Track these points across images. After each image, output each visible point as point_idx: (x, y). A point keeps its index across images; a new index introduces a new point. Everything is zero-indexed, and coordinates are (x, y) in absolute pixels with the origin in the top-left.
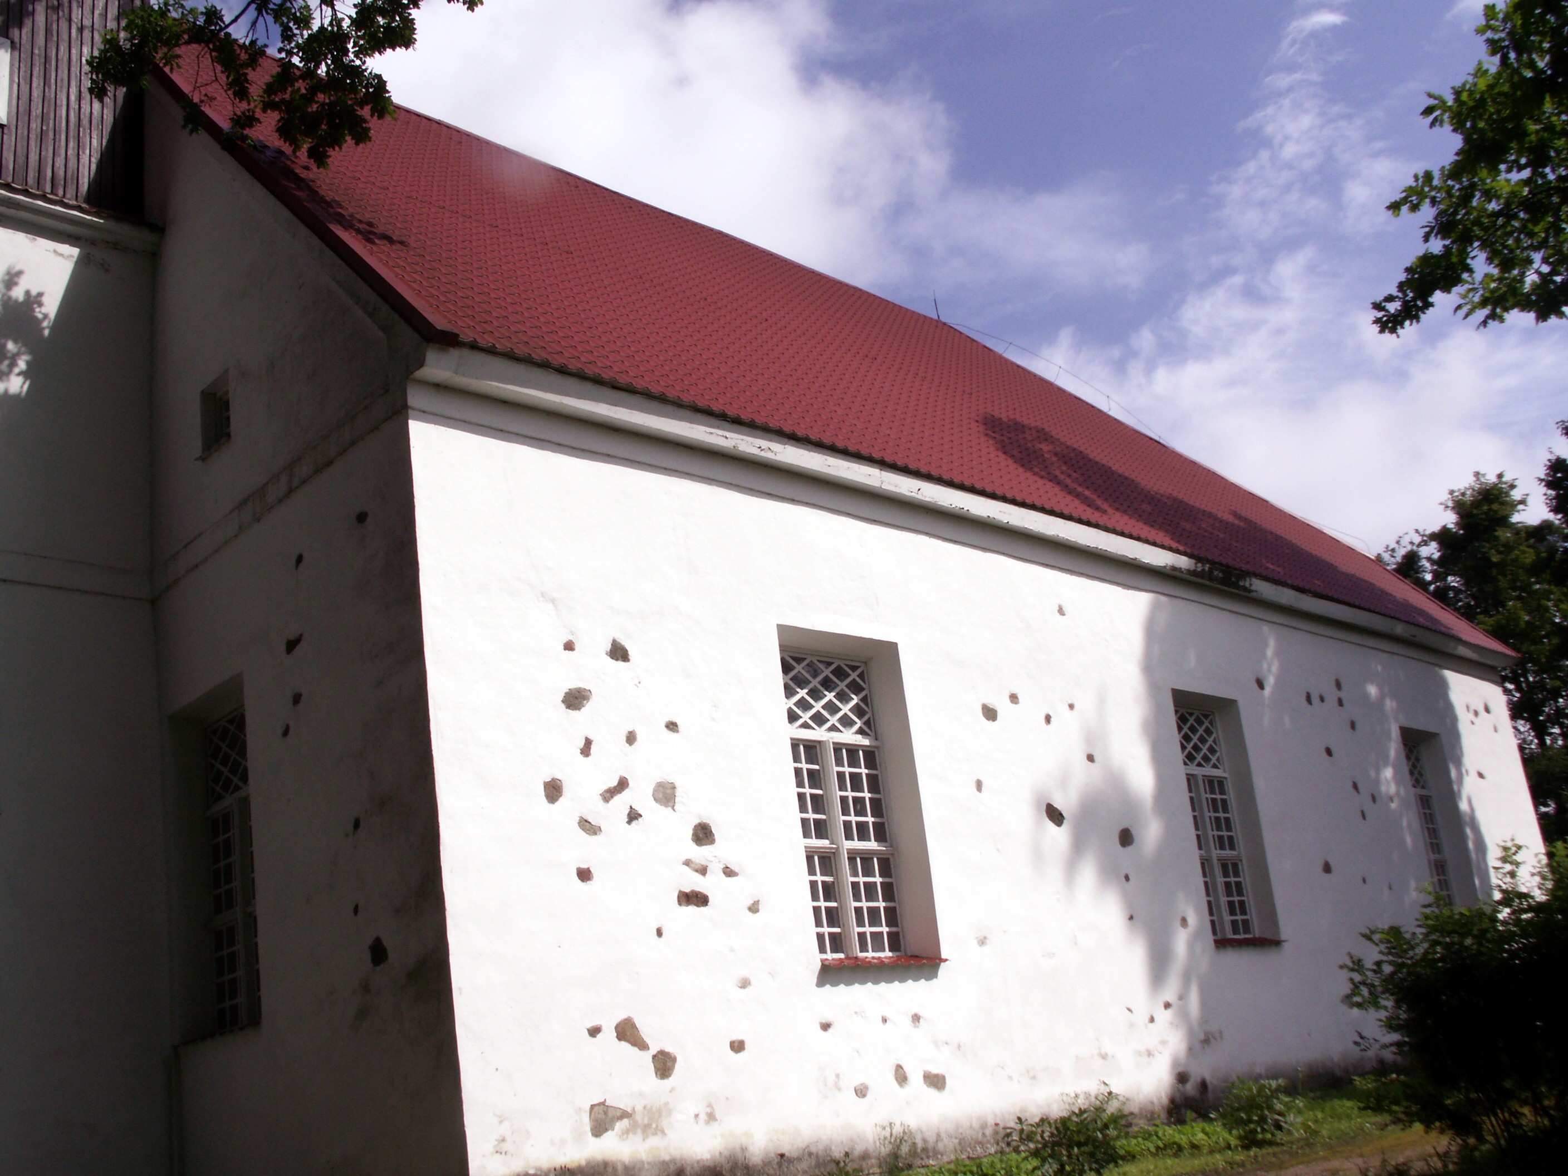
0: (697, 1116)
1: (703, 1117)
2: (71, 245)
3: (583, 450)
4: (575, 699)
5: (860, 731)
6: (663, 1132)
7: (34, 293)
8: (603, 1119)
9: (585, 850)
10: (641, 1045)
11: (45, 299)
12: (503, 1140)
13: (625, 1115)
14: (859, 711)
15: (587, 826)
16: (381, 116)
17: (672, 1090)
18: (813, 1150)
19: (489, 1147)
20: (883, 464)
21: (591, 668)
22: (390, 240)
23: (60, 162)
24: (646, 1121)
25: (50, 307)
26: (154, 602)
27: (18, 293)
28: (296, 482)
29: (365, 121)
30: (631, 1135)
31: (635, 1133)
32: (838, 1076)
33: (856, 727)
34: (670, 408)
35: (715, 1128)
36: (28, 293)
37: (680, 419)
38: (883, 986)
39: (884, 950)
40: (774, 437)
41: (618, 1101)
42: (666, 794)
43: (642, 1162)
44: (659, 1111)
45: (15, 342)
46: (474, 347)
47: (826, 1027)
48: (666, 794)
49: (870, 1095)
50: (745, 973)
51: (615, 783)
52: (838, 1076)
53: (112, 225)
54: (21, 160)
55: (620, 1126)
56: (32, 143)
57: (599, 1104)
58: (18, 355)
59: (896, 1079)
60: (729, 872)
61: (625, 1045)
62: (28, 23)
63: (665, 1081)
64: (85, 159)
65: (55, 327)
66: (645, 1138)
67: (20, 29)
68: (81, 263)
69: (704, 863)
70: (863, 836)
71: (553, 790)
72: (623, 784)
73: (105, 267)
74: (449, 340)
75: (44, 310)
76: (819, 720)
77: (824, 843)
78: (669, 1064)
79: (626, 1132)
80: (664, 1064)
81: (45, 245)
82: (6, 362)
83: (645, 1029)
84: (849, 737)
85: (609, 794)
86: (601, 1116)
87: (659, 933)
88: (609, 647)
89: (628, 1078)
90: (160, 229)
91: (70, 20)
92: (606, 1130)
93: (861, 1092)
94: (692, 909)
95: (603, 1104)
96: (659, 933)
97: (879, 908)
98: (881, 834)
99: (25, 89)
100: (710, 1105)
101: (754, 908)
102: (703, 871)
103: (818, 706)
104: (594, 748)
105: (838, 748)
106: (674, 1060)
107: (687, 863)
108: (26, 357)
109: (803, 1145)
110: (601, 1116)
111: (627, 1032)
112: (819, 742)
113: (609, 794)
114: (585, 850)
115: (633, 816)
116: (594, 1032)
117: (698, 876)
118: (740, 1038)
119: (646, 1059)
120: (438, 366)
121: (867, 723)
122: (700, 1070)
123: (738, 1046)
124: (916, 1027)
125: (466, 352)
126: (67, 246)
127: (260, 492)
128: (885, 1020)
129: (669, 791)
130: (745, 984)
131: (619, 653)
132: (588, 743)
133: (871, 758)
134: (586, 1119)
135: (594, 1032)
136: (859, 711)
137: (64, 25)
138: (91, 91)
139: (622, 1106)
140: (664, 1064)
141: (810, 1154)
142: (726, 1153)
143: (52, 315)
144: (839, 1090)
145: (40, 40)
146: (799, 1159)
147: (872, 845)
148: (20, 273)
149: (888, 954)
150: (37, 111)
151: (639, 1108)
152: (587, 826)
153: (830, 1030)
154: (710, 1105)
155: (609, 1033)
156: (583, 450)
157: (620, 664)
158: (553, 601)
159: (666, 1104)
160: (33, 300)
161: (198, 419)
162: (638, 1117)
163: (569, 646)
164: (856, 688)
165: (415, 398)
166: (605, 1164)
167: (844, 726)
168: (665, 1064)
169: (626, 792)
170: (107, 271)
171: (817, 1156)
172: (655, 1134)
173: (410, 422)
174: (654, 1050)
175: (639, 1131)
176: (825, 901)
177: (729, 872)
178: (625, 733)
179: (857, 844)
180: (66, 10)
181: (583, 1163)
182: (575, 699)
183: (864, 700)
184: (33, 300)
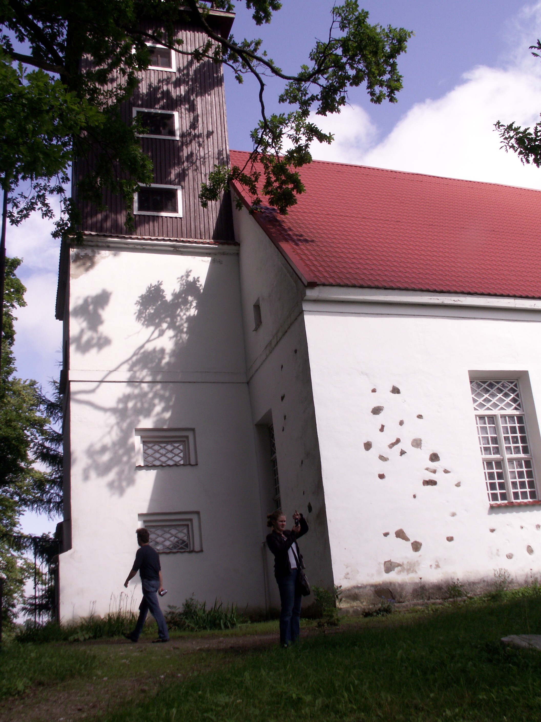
0: (431, 566)
1: (434, 566)
2: (208, 257)
3: (377, 314)
4: (377, 411)
5: (516, 409)
6: (416, 572)
7: (196, 278)
8: (389, 567)
9: (382, 467)
10: (407, 539)
11: (200, 279)
12: (348, 574)
13: (399, 565)
14: (514, 400)
15: (382, 458)
16: (300, 193)
17: (420, 556)
18: (485, 579)
19: (342, 576)
20: (515, 297)
21: (384, 397)
22: (306, 241)
23: (202, 226)
24: (408, 567)
25: (202, 282)
26: (248, 383)
27: (191, 279)
28: (278, 339)
29: (295, 196)
30: (402, 573)
31: (403, 572)
32: (498, 550)
33: (513, 407)
34: (411, 292)
35: (439, 570)
36: (194, 278)
37: (413, 296)
38: (535, 512)
39: (527, 498)
40: (461, 295)
41: (396, 559)
42: (417, 443)
43: (406, 583)
44: (414, 564)
45: (191, 296)
46: (324, 285)
47: (492, 531)
48: (417, 443)
49: (514, 558)
50: (453, 510)
51: (394, 441)
52: (498, 550)
53: (221, 246)
54: (189, 229)
55: (397, 569)
56: (192, 222)
57: (388, 561)
58: (192, 301)
59: (528, 551)
60: (446, 471)
61: (399, 540)
62: (187, 179)
63: (417, 553)
64: (211, 223)
65: (204, 289)
66: (408, 573)
67: (184, 181)
68: (213, 262)
69: (435, 469)
70: (518, 452)
71: (368, 446)
72: (398, 441)
73: (220, 262)
74: (312, 285)
75: (200, 283)
76: (495, 405)
77: (498, 456)
78: (419, 546)
79: (400, 572)
80: (416, 546)
81: (198, 259)
82: (189, 305)
83: (408, 533)
84: (510, 411)
85: (392, 445)
86: (389, 566)
87: (415, 496)
88: (391, 389)
89: (401, 552)
90: (238, 244)
91: (201, 173)
92: (391, 571)
93: (510, 557)
94: (429, 487)
95: (390, 561)
96: (415, 496)
97: (525, 481)
98: (525, 450)
99: (188, 202)
100: (437, 562)
101: (458, 485)
102: (434, 472)
103: (494, 400)
104: (385, 428)
105: (503, 416)
106: (421, 545)
107: (427, 469)
108: (195, 302)
109: (480, 578)
110: (389, 566)
111: (400, 534)
112: (495, 415)
113: (392, 445)
114: (382, 467)
115: (403, 453)
116: (386, 535)
117: (432, 474)
118: (451, 536)
119: (409, 544)
120: (311, 293)
121: (519, 405)
122: (433, 549)
123: (450, 539)
124: (538, 530)
125: (321, 288)
126: (206, 258)
127: (270, 343)
128: (522, 528)
129: (419, 442)
130: (454, 515)
131: (396, 391)
132: (383, 426)
133: (520, 419)
134: (382, 566)
135: (386, 535)
136: (514, 400)
137: (199, 175)
138: (202, 206)
139: (398, 562)
140: (416, 546)
141: (484, 581)
142: (444, 580)
143: (203, 285)
144: (498, 555)
145: (191, 183)
146: (479, 583)
147: (522, 455)
148: (190, 271)
149: (530, 500)
150: (192, 209)
151: (405, 562)
152: (383, 458)
153: (495, 532)
154: (437, 562)
155: (392, 535)
156: (377, 314)
157: (397, 395)
158: (366, 374)
159: (417, 561)
160: (196, 281)
161: (253, 315)
162: (405, 566)
163: (374, 391)
164: (513, 391)
165: (306, 307)
166: (391, 583)
167: (507, 407)
168: (417, 546)
169: (399, 444)
170: (221, 263)
171: (487, 582)
172: (412, 572)
173: (305, 316)
174: (412, 541)
175: (405, 571)
176: (498, 479)
177: (446, 471)
178: (399, 421)
179: (514, 456)
180: (199, 169)
181: (381, 583)
182: (377, 411)
183: (517, 395)
184: (196, 281)
